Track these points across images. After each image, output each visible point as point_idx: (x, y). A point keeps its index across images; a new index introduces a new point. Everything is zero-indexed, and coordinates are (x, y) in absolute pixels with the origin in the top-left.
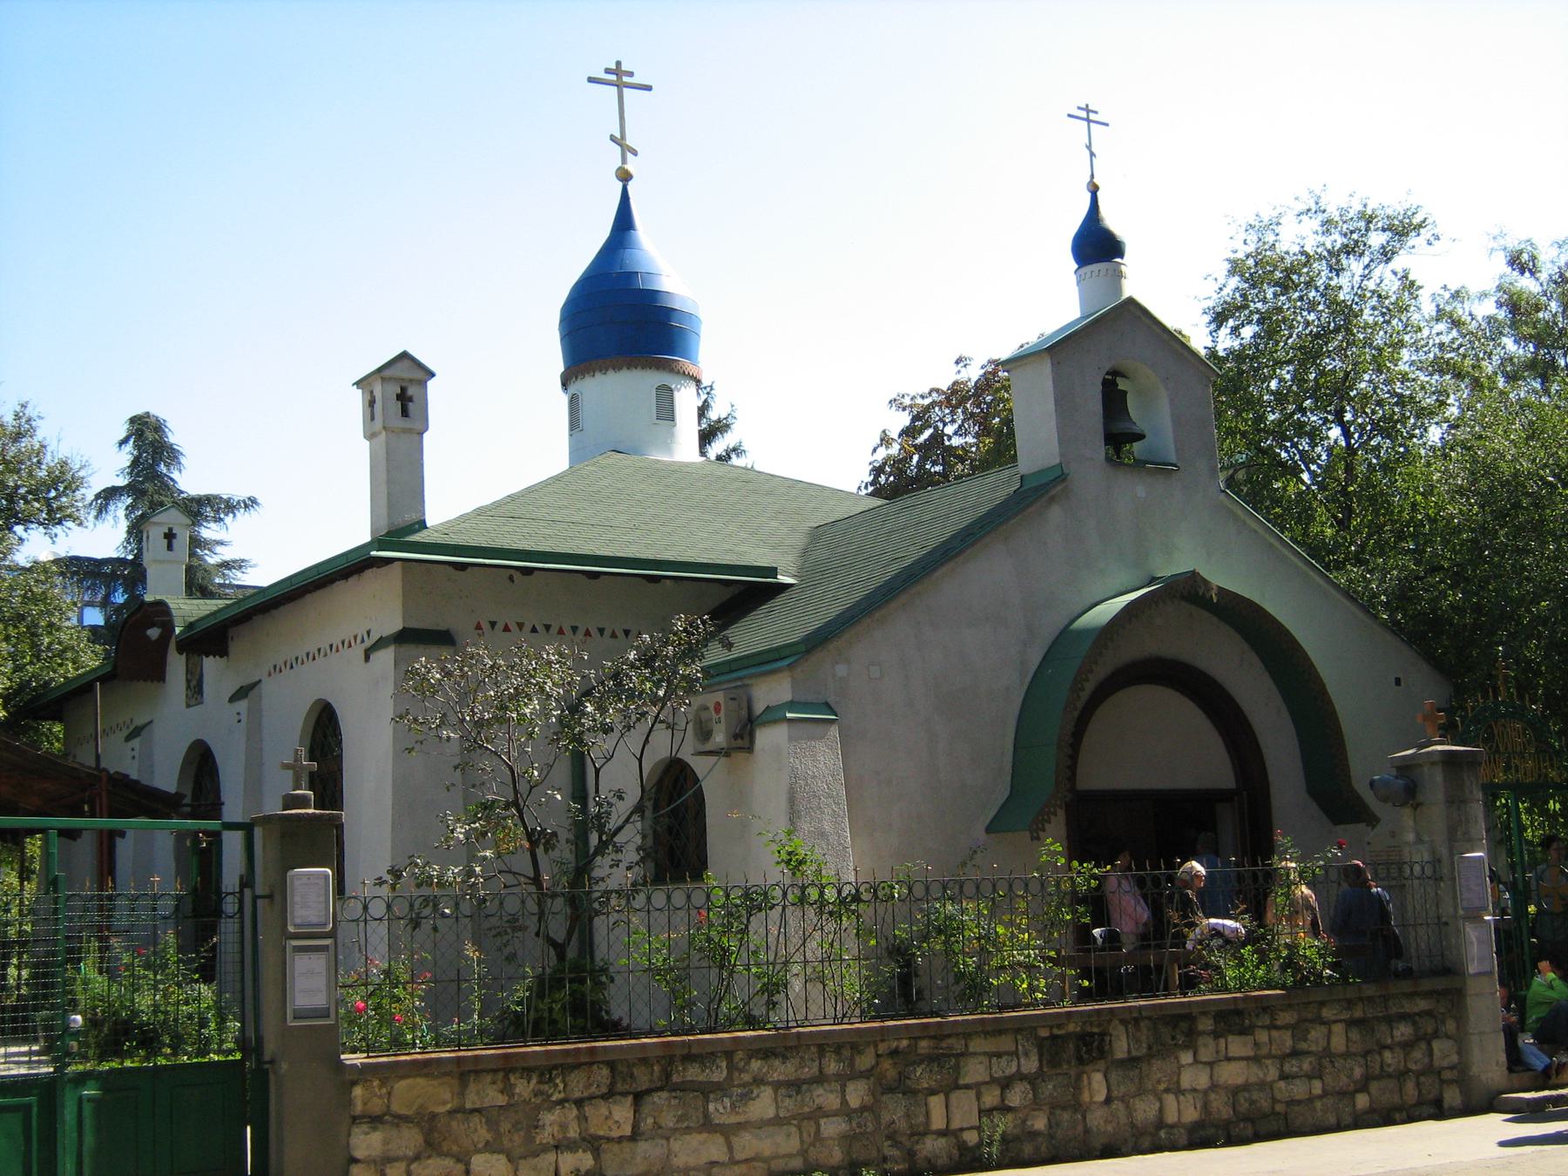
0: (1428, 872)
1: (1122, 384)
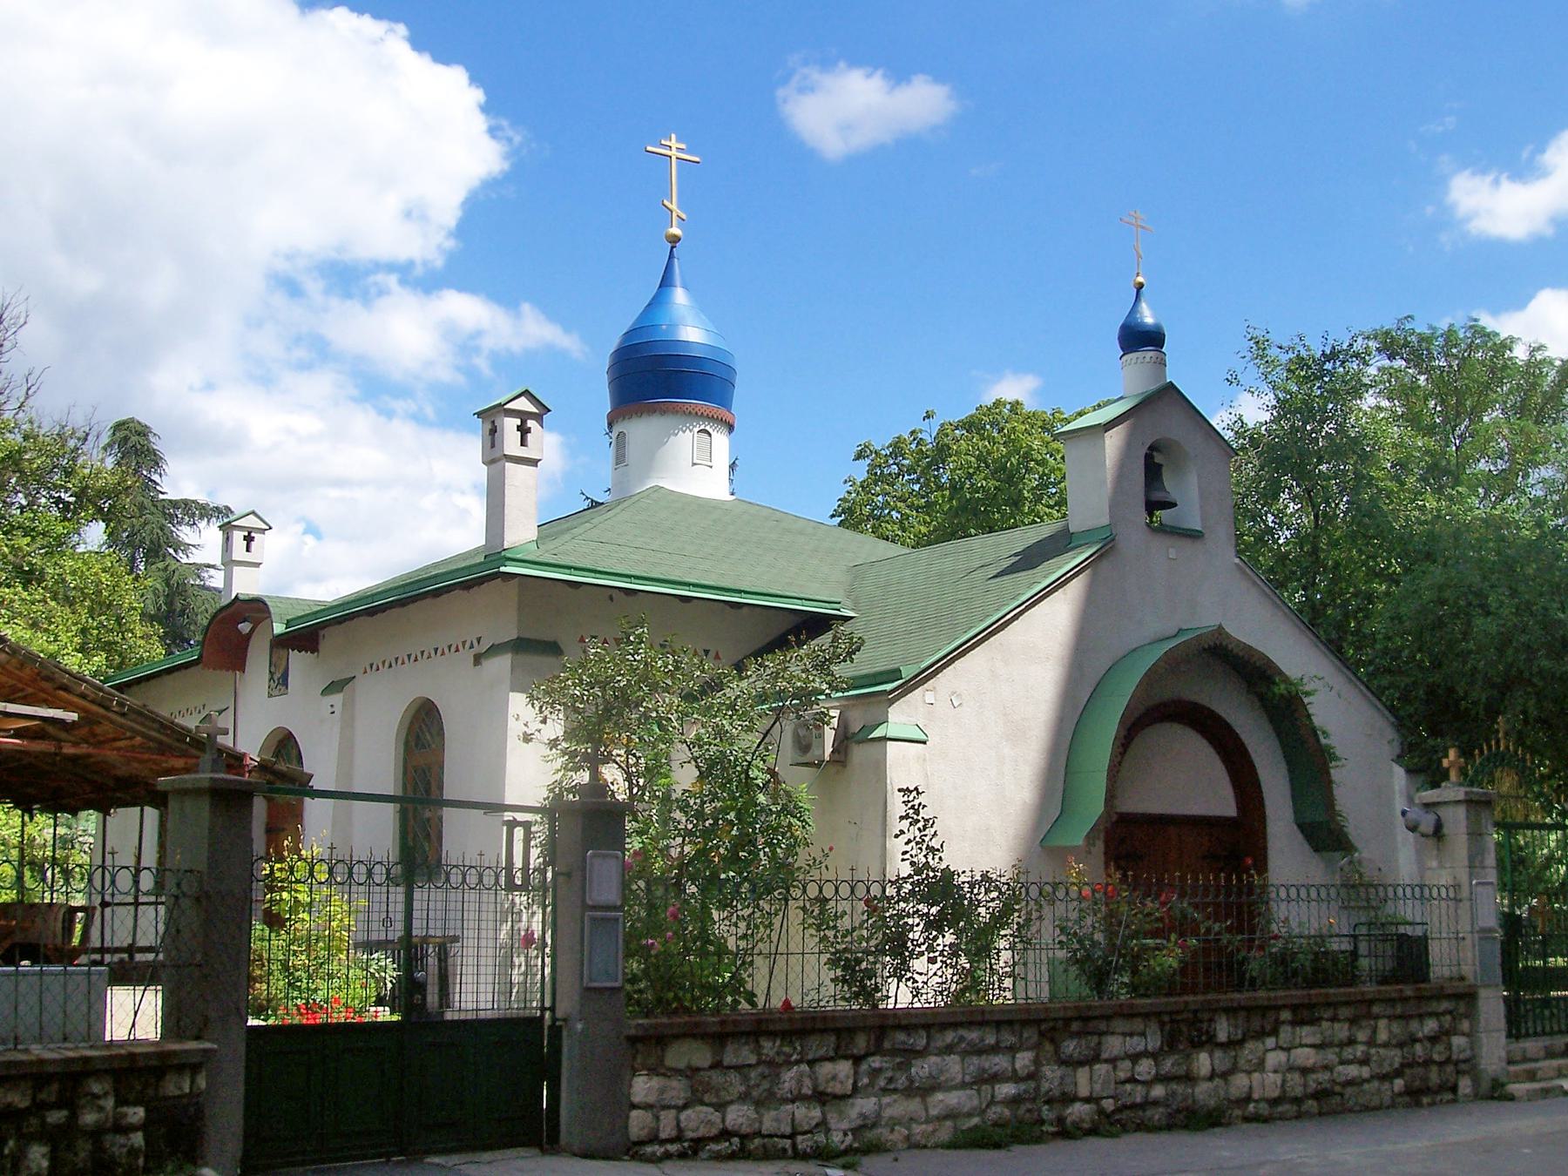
0: (1452, 895)
1: (1158, 458)
